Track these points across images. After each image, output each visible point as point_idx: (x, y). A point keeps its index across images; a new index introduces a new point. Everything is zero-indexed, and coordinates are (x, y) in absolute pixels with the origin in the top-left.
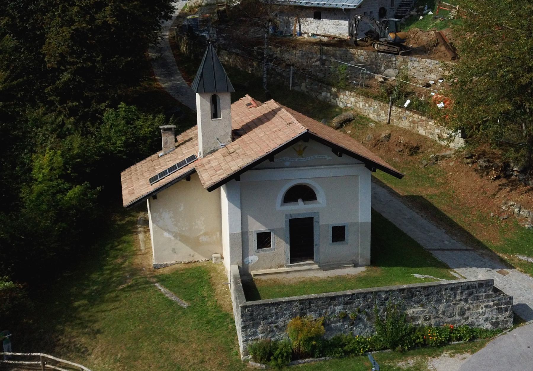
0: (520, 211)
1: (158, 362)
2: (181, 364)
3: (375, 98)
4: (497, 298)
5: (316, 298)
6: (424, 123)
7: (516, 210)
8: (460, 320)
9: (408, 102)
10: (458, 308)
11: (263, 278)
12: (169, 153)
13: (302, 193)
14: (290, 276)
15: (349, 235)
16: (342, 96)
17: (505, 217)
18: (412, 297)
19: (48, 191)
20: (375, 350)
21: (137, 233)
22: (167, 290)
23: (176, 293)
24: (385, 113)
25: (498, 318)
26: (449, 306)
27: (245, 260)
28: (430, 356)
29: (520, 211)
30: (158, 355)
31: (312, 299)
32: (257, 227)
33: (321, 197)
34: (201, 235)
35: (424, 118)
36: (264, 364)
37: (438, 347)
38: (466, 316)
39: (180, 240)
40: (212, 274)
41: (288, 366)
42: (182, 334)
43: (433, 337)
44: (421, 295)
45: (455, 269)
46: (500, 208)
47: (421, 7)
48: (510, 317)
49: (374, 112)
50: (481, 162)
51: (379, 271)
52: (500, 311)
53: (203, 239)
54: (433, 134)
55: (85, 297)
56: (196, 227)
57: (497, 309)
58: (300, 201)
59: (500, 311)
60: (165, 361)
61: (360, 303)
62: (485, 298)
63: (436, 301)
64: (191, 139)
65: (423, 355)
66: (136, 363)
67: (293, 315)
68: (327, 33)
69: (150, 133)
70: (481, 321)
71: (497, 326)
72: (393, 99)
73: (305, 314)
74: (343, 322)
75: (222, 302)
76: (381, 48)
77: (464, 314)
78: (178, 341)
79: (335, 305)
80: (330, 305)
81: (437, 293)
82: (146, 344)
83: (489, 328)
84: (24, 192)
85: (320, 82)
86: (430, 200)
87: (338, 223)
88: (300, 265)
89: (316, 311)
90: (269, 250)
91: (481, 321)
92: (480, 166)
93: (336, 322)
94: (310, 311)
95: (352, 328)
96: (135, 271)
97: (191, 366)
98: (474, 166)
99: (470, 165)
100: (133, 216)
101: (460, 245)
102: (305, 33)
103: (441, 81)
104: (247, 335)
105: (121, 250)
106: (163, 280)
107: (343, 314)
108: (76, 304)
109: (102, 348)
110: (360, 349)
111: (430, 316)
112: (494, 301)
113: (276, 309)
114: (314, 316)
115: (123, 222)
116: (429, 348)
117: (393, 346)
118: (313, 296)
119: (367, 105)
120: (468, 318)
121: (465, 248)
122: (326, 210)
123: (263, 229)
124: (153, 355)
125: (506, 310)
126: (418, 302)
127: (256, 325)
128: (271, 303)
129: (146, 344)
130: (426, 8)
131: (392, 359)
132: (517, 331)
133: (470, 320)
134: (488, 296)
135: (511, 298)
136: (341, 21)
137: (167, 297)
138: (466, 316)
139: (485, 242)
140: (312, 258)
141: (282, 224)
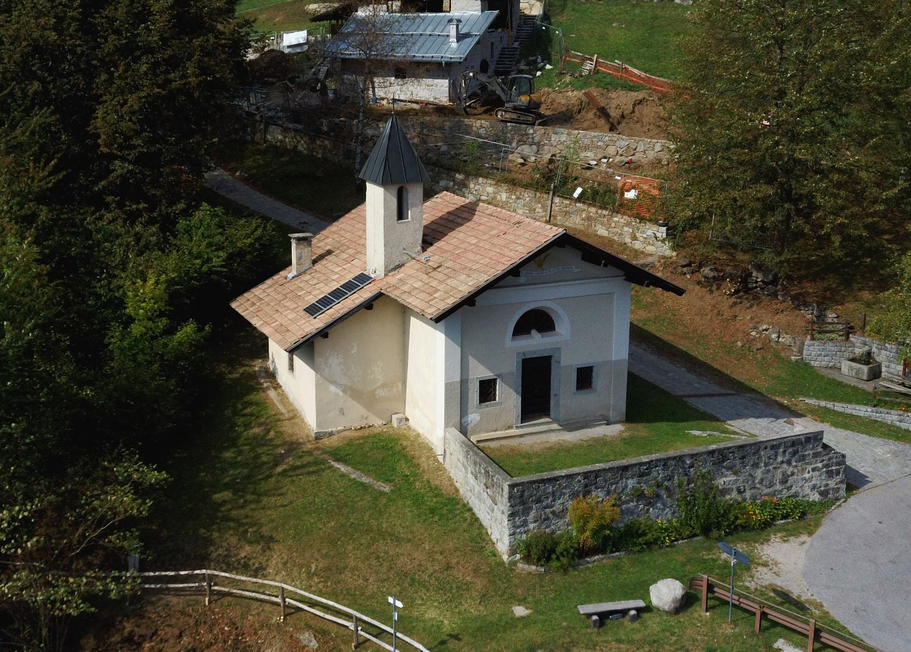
0: (779, 337)
1: (377, 572)
2: (415, 574)
3: (526, 186)
4: (827, 457)
5: (604, 470)
6: (605, 219)
7: (774, 336)
8: (781, 491)
9: (579, 190)
10: (779, 475)
11: (492, 445)
12: (304, 272)
13: (538, 321)
14: (527, 441)
15: (598, 380)
16: (472, 186)
17: (759, 346)
18: (724, 461)
19: (146, 334)
20: (683, 539)
21: (264, 390)
22: (349, 468)
23: (367, 473)
24: (543, 207)
25: (827, 485)
26: (769, 471)
27: (463, 421)
28: (756, 542)
29: (779, 337)
30: (374, 562)
31: (599, 471)
32: (480, 372)
33: (563, 328)
34: (379, 387)
35: (605, 212)
36: (542, 566)
37: (762, 529)
38: (788, 484)
39: (350, 396)
40: (405, 443)
41: (574, 567)
42: (401, 530)
43: (759, 516)
44: (734, 458)
45: (729, 422)
46: (749, 334)
47: (531, 58)
48: (841, 482)
49: (524, 206)
50: (706, 271)
51: (641, 430)
52: (830, 474)
53: (380, 393)
54: (621, 234)
55: (227, 487)
56: (372, 376)
57: (827, 472)
58: (534, 332)
59: (830, 474)
60: (389, 571)
61: (659, 473)
62: (813, 457)
63: (753, 466)
64: (329, 252)
65: (748, 541)
66: (343, 576)
67: (574, 495)
68: (415, 98)
69: (249, 247)
70: (807, 491)
71: (826, 497)
72: (555, 187)
73: (589, 492)
74: (637, 501)
75: (437, 482)
76: (507, 116)
77: (786, 482)
78: (398, 540)
79: (627, 479)
80: (621, 478)
81: (754, 454)
82: (350, 547)
83: (817, 500)
84: (114, 338)
85: (436, 166)
86: (646, 328)
87: (584, 362)
88: (534, 425)
89: (603, 488)
90: (494, 405)
91: (807, 491)
92: (705, 277)
93: (627, 502)
94: (597, 488)
95: (648, 510)
96: (293, 447)
97: (432, 574)
98: (695, 278)
99: (688, 277)
100: (247, 365)
101: (716, 389)
102: (383, 99)
103: (605, 160)
104: (515, 527)
105: (252, 415)
106: (338, 455)
107: (637, 490)
108: (217, 497)
109: (282, 559)
110: (664, 538)
111: (744, 487)
112: (823, 461)
113: (553, 487)
114: (600, 494)
115: (235, 376)
116: (749, 531)
117: (706, 531)
118: (599, 466)
119: (514, 197)
120: (791, 486)
121: (723, 391)
122: (568, 346)
123: (487, 374)
124: (367, 563)
125: (838, 473)
126: (729, 468)
127: (526, 512)
128: (548, 479)
129: (350, 547)
130: (539, 60)
131: (709, 549)
132: (852, 500)
133: (793, 490)
134: (816, 455)
135: (844, 456)
136: (436, 81)
137: (354, 479)
138: (788, 484)
139: (747, 383)
140: (548, 415)
141: (513, 367)
